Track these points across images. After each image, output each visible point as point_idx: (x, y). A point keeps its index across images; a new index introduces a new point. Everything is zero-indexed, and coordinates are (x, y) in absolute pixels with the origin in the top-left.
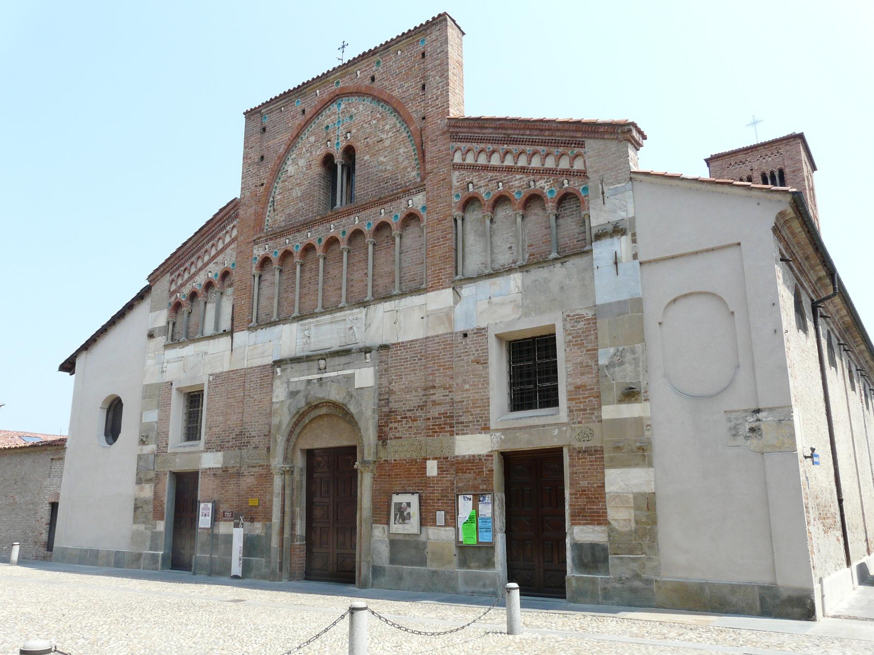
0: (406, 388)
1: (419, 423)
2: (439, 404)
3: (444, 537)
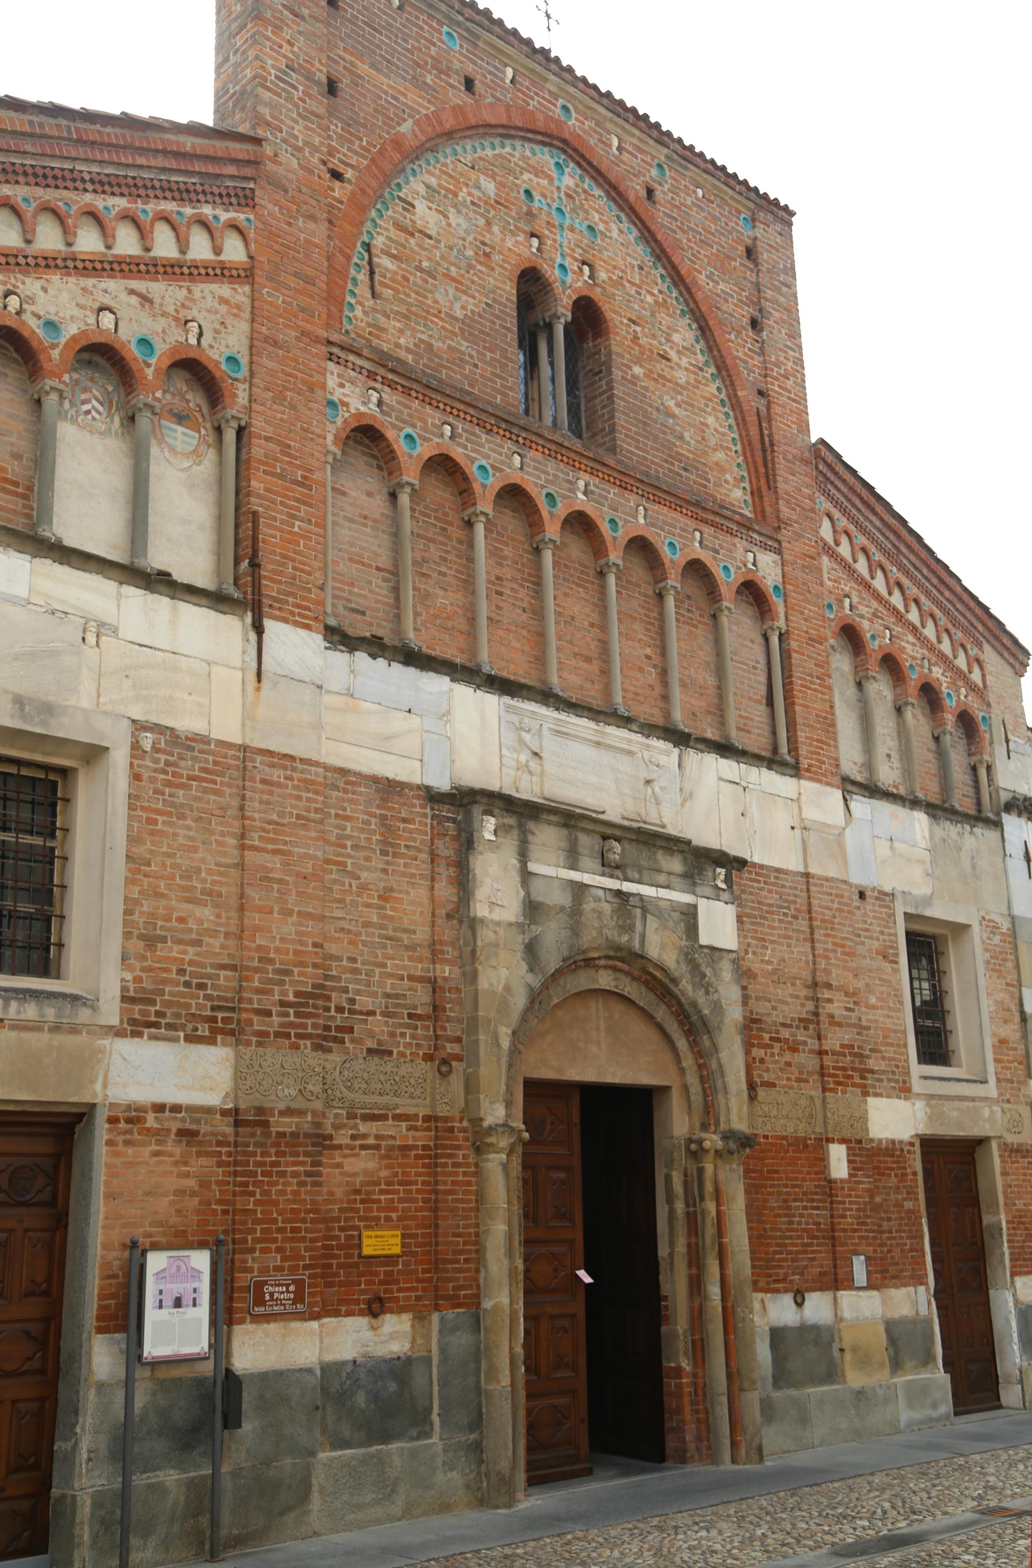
1: (800, 1058)
2: (840, 1025)
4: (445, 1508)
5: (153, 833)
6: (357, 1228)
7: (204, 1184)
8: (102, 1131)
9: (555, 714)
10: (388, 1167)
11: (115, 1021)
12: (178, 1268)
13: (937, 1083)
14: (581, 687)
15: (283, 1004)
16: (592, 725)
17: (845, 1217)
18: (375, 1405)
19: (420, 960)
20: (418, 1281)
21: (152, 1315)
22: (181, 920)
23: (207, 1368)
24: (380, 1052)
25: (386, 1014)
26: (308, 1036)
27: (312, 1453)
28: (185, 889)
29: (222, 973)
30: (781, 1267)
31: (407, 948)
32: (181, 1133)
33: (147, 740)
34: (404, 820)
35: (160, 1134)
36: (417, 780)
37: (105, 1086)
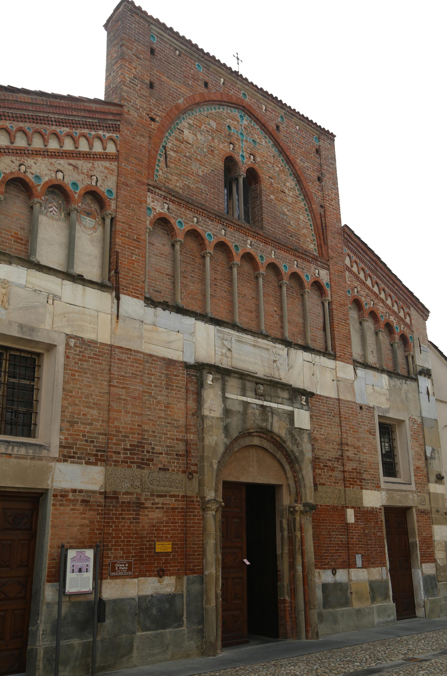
0: (325, 438)
1: (335, 474)
2: (351, 460)
3: (362, 578)
4: (188, 656)
5: (74, 379)
6: (154, 541)
7: (92, 522)
8: (51, 500)
9: (237, 334)
10: (167, 516)
11: (57, 455)
12: (81, 556)
13: (391, 484)
14: (248, 323)
15: (125, 449)
16: (252, 338)
17: (353, 538)
18: (159, 614)
19: (181, 432)
20: (178, 563)
21: (69, 575)
22: (84, 415)
23: (92, 597)
24: (164, 469)
25: (167, 454)
26: (135, 463)
27: (134, 633)
28: (86, 402)
29: (101, 436)
30: (327, 559)
31: (176, 427)
32: (83, 501)
33: (72, 342)
34: (176, 376)
35: (74, 501)
36: (181, 359)
37: (52, 482)
